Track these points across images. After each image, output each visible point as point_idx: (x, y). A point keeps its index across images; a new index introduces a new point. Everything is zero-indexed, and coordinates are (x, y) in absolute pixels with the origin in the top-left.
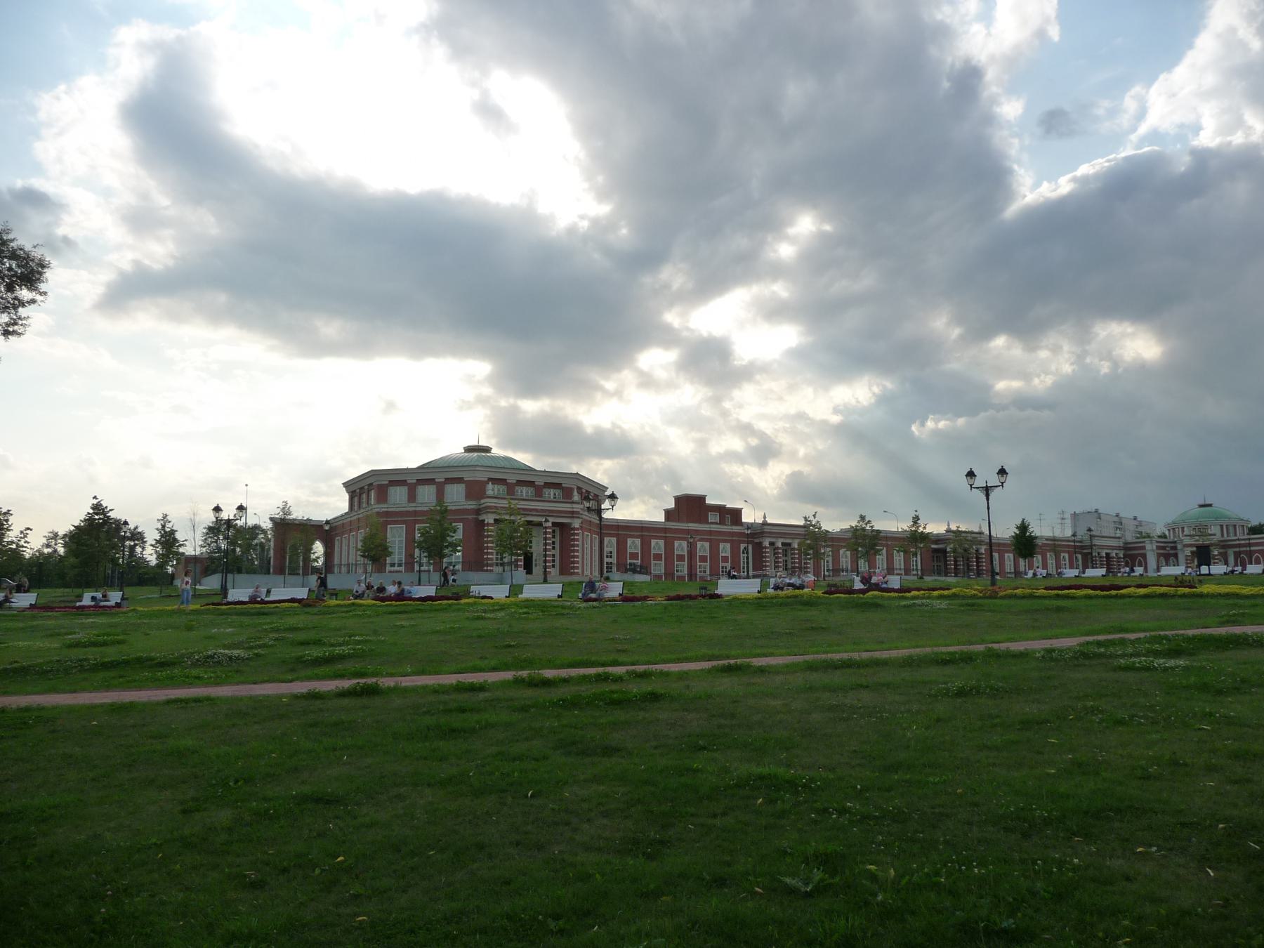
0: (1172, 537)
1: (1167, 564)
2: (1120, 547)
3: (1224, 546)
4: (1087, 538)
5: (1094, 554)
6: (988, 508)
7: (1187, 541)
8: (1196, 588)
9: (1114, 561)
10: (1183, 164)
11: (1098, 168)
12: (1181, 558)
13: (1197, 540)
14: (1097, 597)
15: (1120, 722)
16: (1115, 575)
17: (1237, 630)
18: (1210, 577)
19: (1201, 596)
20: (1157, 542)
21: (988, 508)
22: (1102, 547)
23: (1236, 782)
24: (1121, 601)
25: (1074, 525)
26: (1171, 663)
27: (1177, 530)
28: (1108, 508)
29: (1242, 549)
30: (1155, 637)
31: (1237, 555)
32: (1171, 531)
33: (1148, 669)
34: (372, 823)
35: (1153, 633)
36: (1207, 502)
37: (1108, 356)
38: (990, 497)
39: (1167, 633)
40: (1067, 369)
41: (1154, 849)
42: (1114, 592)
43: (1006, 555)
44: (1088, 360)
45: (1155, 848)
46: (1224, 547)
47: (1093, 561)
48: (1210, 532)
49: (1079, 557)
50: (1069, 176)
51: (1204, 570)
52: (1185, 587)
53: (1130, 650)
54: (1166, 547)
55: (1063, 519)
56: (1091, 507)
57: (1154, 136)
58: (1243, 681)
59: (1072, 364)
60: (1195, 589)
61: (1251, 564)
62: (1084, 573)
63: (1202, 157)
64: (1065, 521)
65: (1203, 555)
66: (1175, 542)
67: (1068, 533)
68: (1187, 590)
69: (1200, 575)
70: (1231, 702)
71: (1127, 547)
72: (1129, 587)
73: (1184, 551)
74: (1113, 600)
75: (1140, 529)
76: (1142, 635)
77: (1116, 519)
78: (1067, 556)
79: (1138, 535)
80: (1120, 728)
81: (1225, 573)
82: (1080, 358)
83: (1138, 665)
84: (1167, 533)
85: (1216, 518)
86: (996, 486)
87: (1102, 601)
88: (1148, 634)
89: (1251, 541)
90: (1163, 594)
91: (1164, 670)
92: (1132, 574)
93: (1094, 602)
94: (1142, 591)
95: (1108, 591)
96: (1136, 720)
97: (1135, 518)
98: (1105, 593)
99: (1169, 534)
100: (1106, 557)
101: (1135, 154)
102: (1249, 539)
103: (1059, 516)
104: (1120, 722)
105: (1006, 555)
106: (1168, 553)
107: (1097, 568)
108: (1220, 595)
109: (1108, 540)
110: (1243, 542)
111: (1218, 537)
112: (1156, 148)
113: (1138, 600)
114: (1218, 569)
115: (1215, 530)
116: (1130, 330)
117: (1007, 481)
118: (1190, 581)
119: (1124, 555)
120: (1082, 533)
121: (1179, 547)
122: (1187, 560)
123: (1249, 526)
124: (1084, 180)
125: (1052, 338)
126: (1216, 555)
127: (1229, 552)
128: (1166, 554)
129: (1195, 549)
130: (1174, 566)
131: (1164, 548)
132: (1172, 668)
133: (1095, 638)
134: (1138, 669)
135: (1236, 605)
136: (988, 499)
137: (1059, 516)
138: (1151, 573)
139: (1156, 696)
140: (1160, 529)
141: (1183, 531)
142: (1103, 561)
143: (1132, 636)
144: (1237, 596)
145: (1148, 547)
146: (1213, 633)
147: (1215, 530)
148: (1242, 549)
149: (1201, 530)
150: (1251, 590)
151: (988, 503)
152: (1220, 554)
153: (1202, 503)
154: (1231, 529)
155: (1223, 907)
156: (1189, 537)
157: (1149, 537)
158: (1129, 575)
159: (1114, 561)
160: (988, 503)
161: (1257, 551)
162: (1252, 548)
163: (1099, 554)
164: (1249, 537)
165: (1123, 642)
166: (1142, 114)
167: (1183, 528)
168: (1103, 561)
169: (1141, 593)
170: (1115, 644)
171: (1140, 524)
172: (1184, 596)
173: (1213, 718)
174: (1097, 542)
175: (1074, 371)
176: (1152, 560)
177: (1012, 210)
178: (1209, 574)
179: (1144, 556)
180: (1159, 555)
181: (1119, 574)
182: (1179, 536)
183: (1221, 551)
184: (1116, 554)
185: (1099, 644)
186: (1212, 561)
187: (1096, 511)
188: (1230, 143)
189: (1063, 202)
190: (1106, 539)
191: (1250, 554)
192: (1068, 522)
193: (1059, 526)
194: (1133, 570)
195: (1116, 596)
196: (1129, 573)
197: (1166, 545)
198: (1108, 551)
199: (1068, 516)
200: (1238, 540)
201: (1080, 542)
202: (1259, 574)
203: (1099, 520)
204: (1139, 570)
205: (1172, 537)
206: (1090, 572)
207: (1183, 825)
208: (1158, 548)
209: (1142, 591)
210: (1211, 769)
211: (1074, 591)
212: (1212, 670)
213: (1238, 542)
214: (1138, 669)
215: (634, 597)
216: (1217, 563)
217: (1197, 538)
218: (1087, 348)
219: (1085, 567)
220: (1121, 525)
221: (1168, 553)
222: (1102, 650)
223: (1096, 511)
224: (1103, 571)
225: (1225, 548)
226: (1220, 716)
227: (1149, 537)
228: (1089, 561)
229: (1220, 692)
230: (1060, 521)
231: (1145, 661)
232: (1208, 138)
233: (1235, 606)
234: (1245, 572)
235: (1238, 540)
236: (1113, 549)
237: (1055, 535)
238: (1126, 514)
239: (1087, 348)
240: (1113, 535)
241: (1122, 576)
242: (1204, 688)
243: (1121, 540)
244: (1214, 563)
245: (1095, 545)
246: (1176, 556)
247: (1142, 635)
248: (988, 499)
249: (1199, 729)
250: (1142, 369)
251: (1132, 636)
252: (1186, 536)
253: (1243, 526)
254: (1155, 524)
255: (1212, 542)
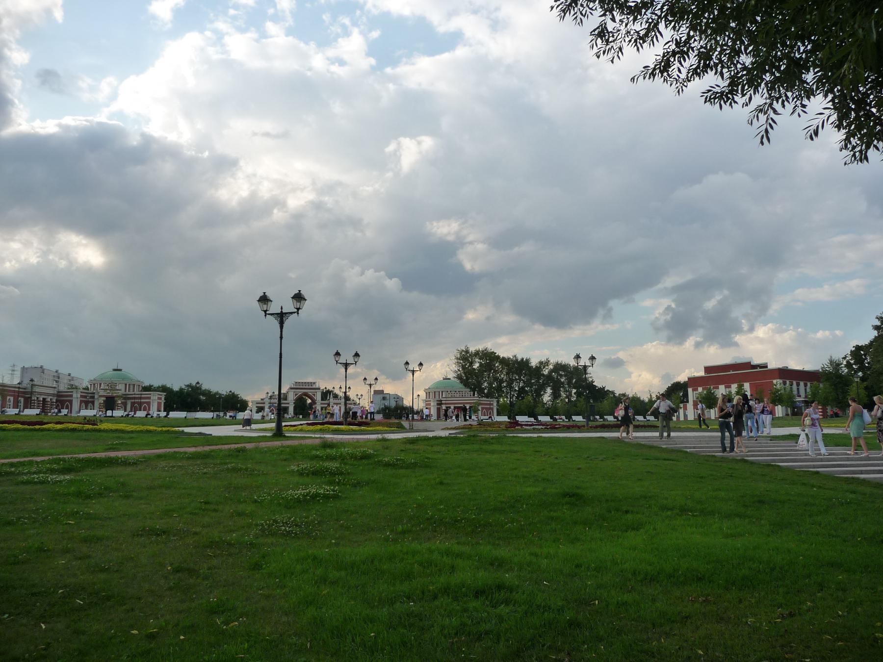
0: (92, 390)
1: (86, 408)
2: (54, 394)
3: (126, 398)
4: (29, 386)
5: (33, 398)
6: (281, 338)
7: (102, 393)
8: (97, 425)
9: (48, 407)
10: (135, 141)
11: (78, 123)
12: (97, 404)
13: (108, 393)
14: (24, 430)
15: (9, 523)
16: (46, 414)
17: (112, 454)
18: (112, 418)
19: (99, 431)
20: (81, 392)
21: (281, 338)
22: (41, 394)
23: (80, 559)
24: (41, 433)
25: (22, 376)
26: (62, 477)
27: (96, 385)
28: (50, 366)
29: (136, 401)
30: (57, 459)
31: (133, 404)
32: (92, 385)
33: (42, 483)
34: (478, 569)
35: (55, 457)
36: (119, 368)
37: (67, 257)
38: (285, 325)
39: (65, 456)
40: (34, 260)
41: (6, 616)
42: (37, 427)
43: (8, 398)
44: (51, 257)
45: (7, 615)
46: (125, 398)
47: (31, 403)
48: (118, 388)
49: (22, 400)
50: (57, 121)
51: (109, 413)
52: (90, 424)
53: (34, 469)
54: (87, 396)
55: (13, 371)
56: (37, 364)
57: (120, 115)
58: (106, 489)
59: (38, 257)
60: (96, 426)
61: (140, 410)
62: (23, 412)
63: (148, 140)
64: (15, 372)
65: (110, 403)
66: (94, 393)
67: (16, 381)
68: (90, 427)
69: (106, 416)
70: (94, 503)
71: (59, 395)
72: (50, 423)
73: (99, 400)
74: (35, 433)
75: (72, 383)
76: (46, 458)
77: (56, 374)
78: (12, 398)
79: (69, 387)
80: (8, 528)
81: (122, 416)
82: (45, 254)
83: (36, 480)
84: (89, 387)
85: (123, 379)
86: (352, 364)
87: (30, 433)
88: (51, 457)
89: (142, 396)
90: (73, 429)
91: (54, 483)
92: (59, 414)
93: (20, 433)
94: (59, 426)
95: (33, 426)
96: (22, 521)
97: (69, 375)
98: (31, 427)
99: (91, 387)
100: (43, 401)
101: (107, 123)
102: (141, 394)
103: (11, 368)
104: (9, 523)
105: (8, 398)
106: (88, 401)
107: (34, 408)
108: (112, 431)
109: (46, 387)
110: (138, 396)
111: (123, 392)
112: (121, 124)
113: (55, 433)
114: (118, 413)
115: (121, 387)
116: (84, 242)
117: (359, 361)
118: (94, 421)
119: (56, 400)
120: (25, 384)
121: (96, 397)
122: (100, 406)
123: (143, 386)
124: (67, 128)
125: (24, 234)
126: (120, 404)
127: (128, 402)
128: (86, 401)
129: (105, 399)
130: (91, 409)
131: (85, 397)
132: (60, 482)
133: (10, 460)
134: (36, 483)
135: (119, 437)
136: (282, 327)
137: (11, 368)
138: (74, 414)
139: (42, 501)
140: (86, 384)
141: (100, 386)
142: (40, 404)
143: (39, 459)
144: (122, 431)
145: (75, 395)
146: (97, 456)
147: (121, 387)
148: (136, 401)
149: (112, 386)
150: (132, 428)
151: (346, 374)
152: (122, 403)
153: (116, 368)
154: (132, 387)
155: (45, 649)
156: (103, 391)
157: (76, 388)
158: (57, 415)
159: (48, 407)
160: (346, 374)
161: (485, 408)
162: (142, 401)
163: (37, 398)
164: (141, 393)
165: (31, 463)
166: (114, 97)
167: (100, 384)
168: (40, 404)
169: (58, 428)
170: (24, 465)
171: (73, 379)
172: (87, 430)
173: (78, 515)
174: (37, 389)
175: (38, 262)
176: (76, 405)
177: (9, 131)
178: (112, 416)
179: (71, 402)
180: (81, 402)
181: (49, 414)
182: (97, 389)
183: (123, 401)
184: (51, 399)
185: (12, 465)
186: (116, 407)
187: (41, 367)
188: (166, 138)
189: (47, 139)
190: (47, 388)
191: (140, 404)
192: (18, 374)
193: (9, 376)
194: (60, 411)
195: (39, 430)
196: (57, 414)
197: (86, 395)
198: (45, 397)
199: (18, 369)
200: (135, 394)
201: (25, 389)
202: (143, 418)
203: (42, 374)
204: (64, 412)
205: (92, 390)
206: (28, 412)
207: (33, 594)
208: (82, 396)
209: (59, 426)
210: (66, 551)
211: (7, 425)
212: (87, 482)
213: (134, 396)
214: (36, 483)
215: (312, 426)
216: (120, 409)
217: (108, 391)
218: (51, 247)
219: (26, 407)
220: (59, 379)
221: (88, 401)
222: (13, 469)
223: (41, 367)
224: (37, 411)
225: (125, 399)
226: (83, 513)
227: (76, 388)
228: (28, 404)
229: (89, 497)
230: (10, 372)
231: (42, 477)
232: (155, 130)
233: (118, 438)
234: (135, 416)
235: (135, 394)
236: (41, 395)
237: (4, 382)
238: (64, 371)
239: (51, 247)
240: (50, 385)
241: (52, 415)
242: (78, 494)
243: (55, 389)
244: (118, 409)
245: (35, 392)
246: (93, 403)
247: (46, 458)
248: (282, 327)
249: (66, 524)
250: (88, 271)
251: (39, 459)
252: (102, 389)
253: (139, 385)
254: (83, 380)
255: (118, 395)
